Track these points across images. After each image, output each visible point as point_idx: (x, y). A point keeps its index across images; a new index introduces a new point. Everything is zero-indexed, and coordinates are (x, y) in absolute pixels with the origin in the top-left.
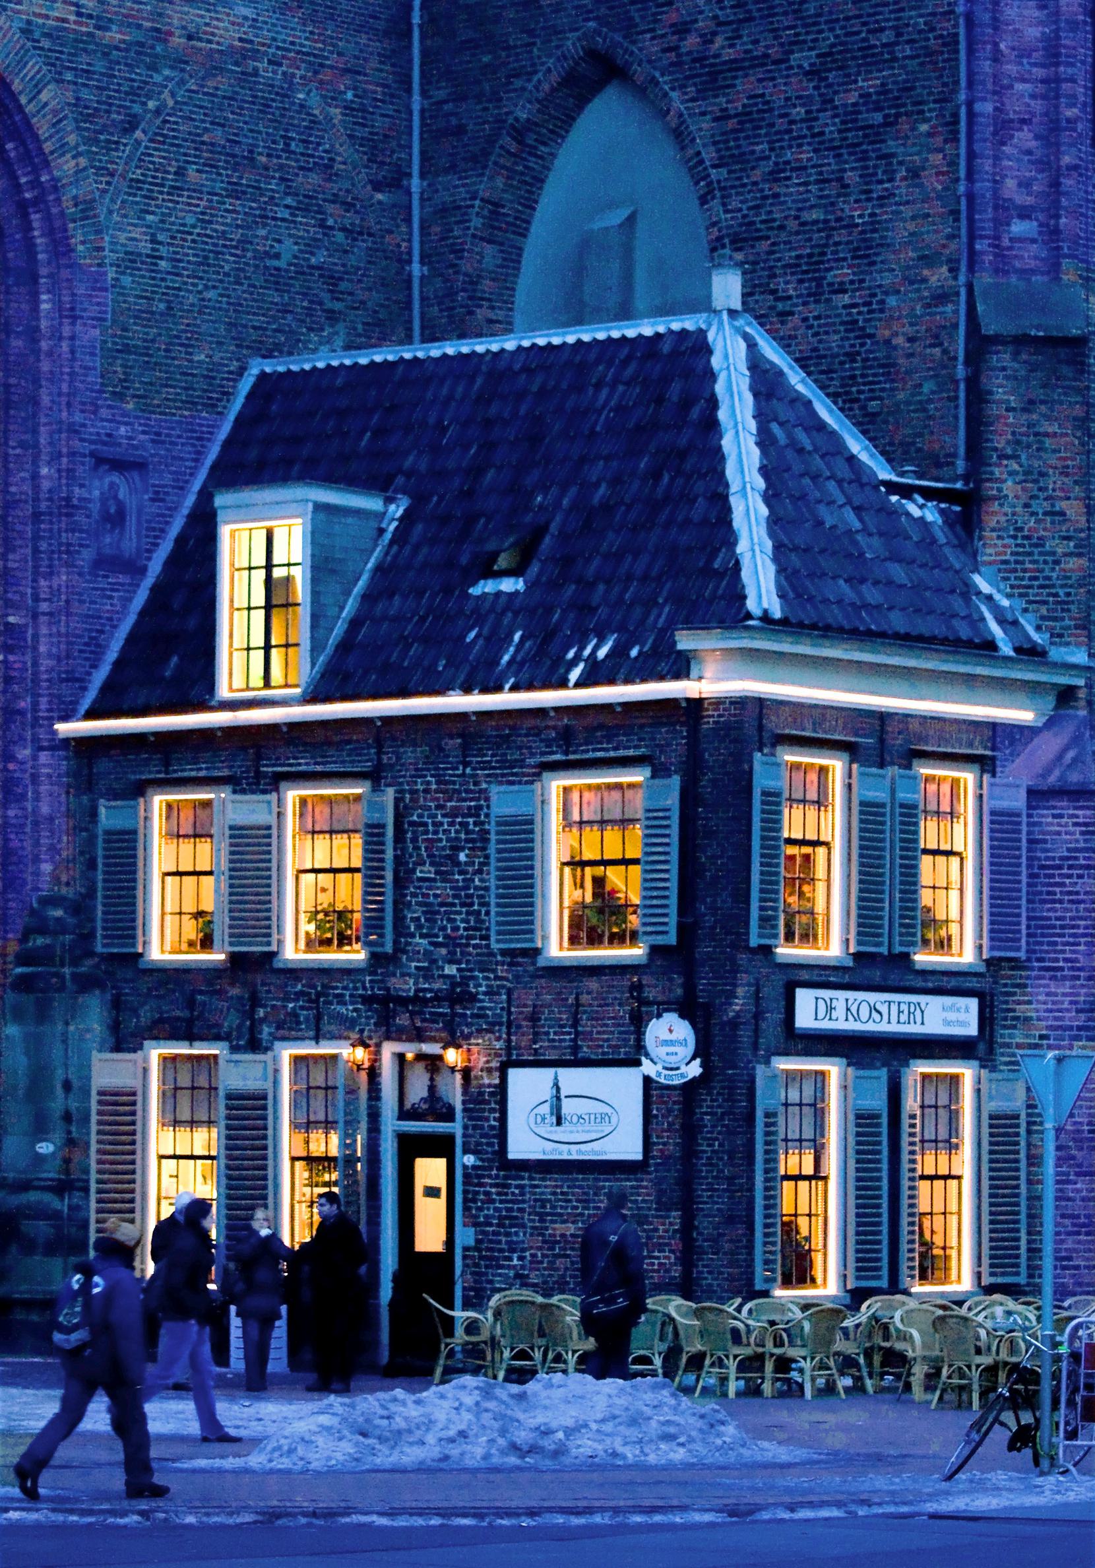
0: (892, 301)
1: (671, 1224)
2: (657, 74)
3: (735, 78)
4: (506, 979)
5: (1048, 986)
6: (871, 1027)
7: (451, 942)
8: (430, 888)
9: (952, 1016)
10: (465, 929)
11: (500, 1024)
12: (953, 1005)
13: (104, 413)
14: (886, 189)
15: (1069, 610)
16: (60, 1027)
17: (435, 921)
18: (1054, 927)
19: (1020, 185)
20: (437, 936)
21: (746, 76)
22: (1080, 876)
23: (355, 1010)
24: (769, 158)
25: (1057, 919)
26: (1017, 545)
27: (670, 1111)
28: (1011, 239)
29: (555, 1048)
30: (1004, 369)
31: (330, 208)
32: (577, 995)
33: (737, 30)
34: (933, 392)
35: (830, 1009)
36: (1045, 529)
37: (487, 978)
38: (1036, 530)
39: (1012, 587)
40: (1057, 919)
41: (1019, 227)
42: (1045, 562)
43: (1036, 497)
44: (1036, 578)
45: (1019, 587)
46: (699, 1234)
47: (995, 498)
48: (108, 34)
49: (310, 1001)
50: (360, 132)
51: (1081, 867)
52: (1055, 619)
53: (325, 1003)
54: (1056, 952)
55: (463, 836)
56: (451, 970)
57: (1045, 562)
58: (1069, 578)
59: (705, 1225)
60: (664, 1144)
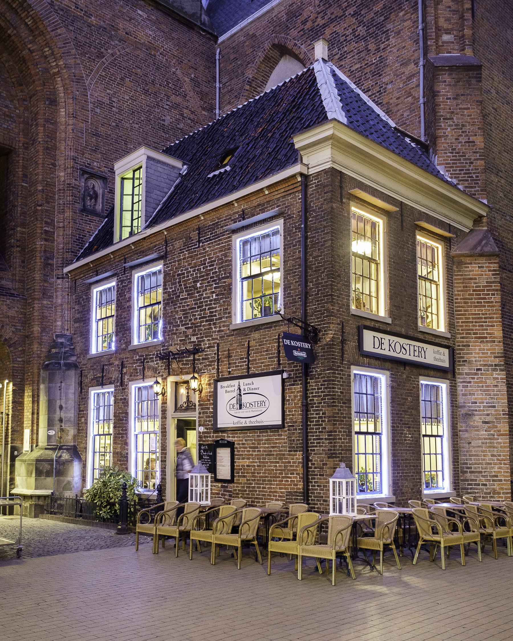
0: (390, 86)
1: (297, 459)
2: (296, 42)
3: (325, 30)
4: (217, 339)
5: (480, 346)
6: (401, 356)
7: (195, 326)
8: (185, 302)
9: (438, 356)
10: (200, 318)
11: (214, 361)
12: (438, 351)
13: (87, 155)
14: (386, 44)
15: (478, 183)
16: (59, 385)
17: (187, 317)
18: (481, 318)
19: (445, 20)
20: (188, 324)
21: (329, 27)
22: (493, 295)
23: (157, 364)
24: (338, 53)
25: (483, 314)
26: (453, 156)
27: (295, 396)
28: (442, 43)
29: (239, 370)
30: (445, 82)
31: (185, 111)
32: (249, 341)
33: (326, 12)
34: (408, 116)
35: (381, 344)
36: (465, 149)
37: (209, 340)
38: (461, 149)
39: (451, 174)
40: (483, 314)
41: (446, 38)
42: (466, 163)
43: (461, 135)
44: (462, 170)
45: (455, 174)
46: (312, 464)
47: (443, 136)
48: (90, 19)
49: (141, 362)
50: (197, 89)
51: (493, 290)
52: (472, 187)
53: (147, 362)
54: (483, 330)
55: (199, 275)
56: (194, 339)
57: (466, 163)
58: (478, 169)
59: (315, 458)
60: (293, 415)
